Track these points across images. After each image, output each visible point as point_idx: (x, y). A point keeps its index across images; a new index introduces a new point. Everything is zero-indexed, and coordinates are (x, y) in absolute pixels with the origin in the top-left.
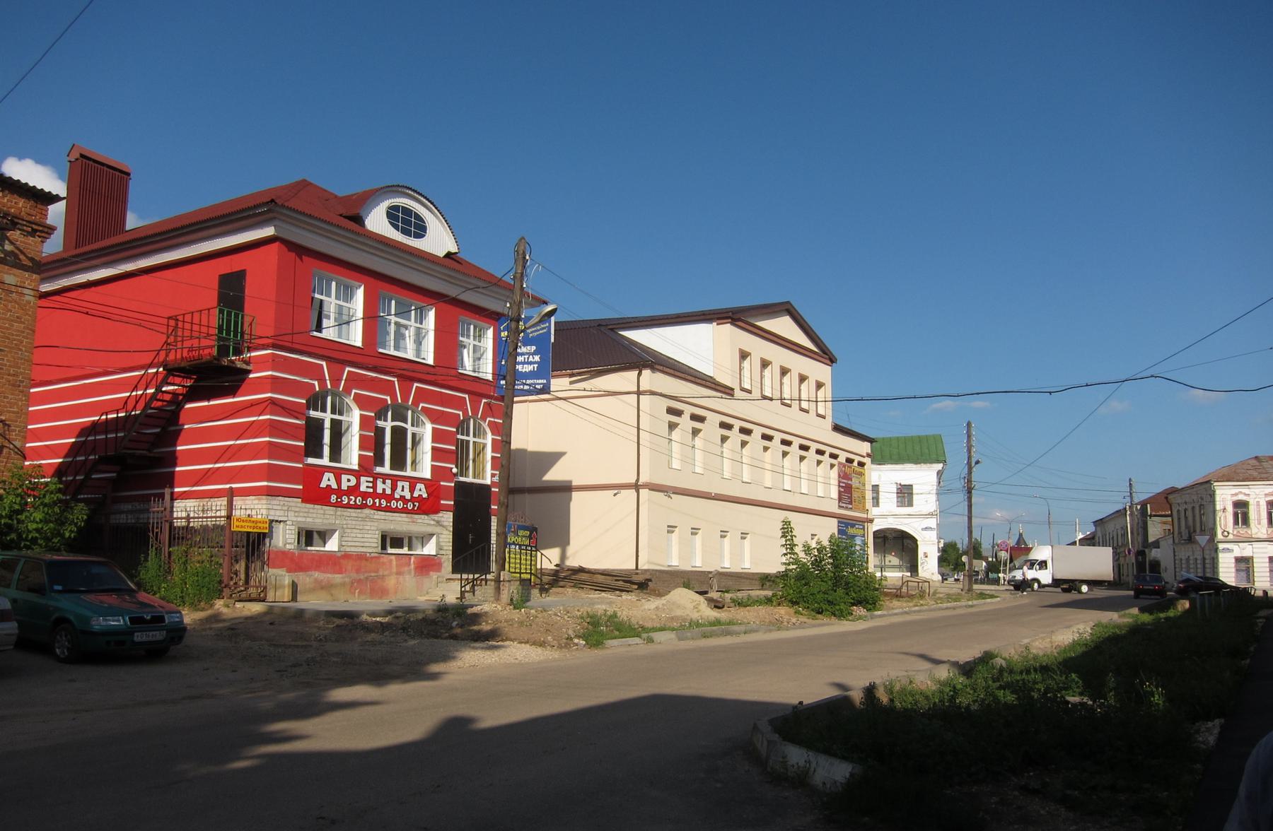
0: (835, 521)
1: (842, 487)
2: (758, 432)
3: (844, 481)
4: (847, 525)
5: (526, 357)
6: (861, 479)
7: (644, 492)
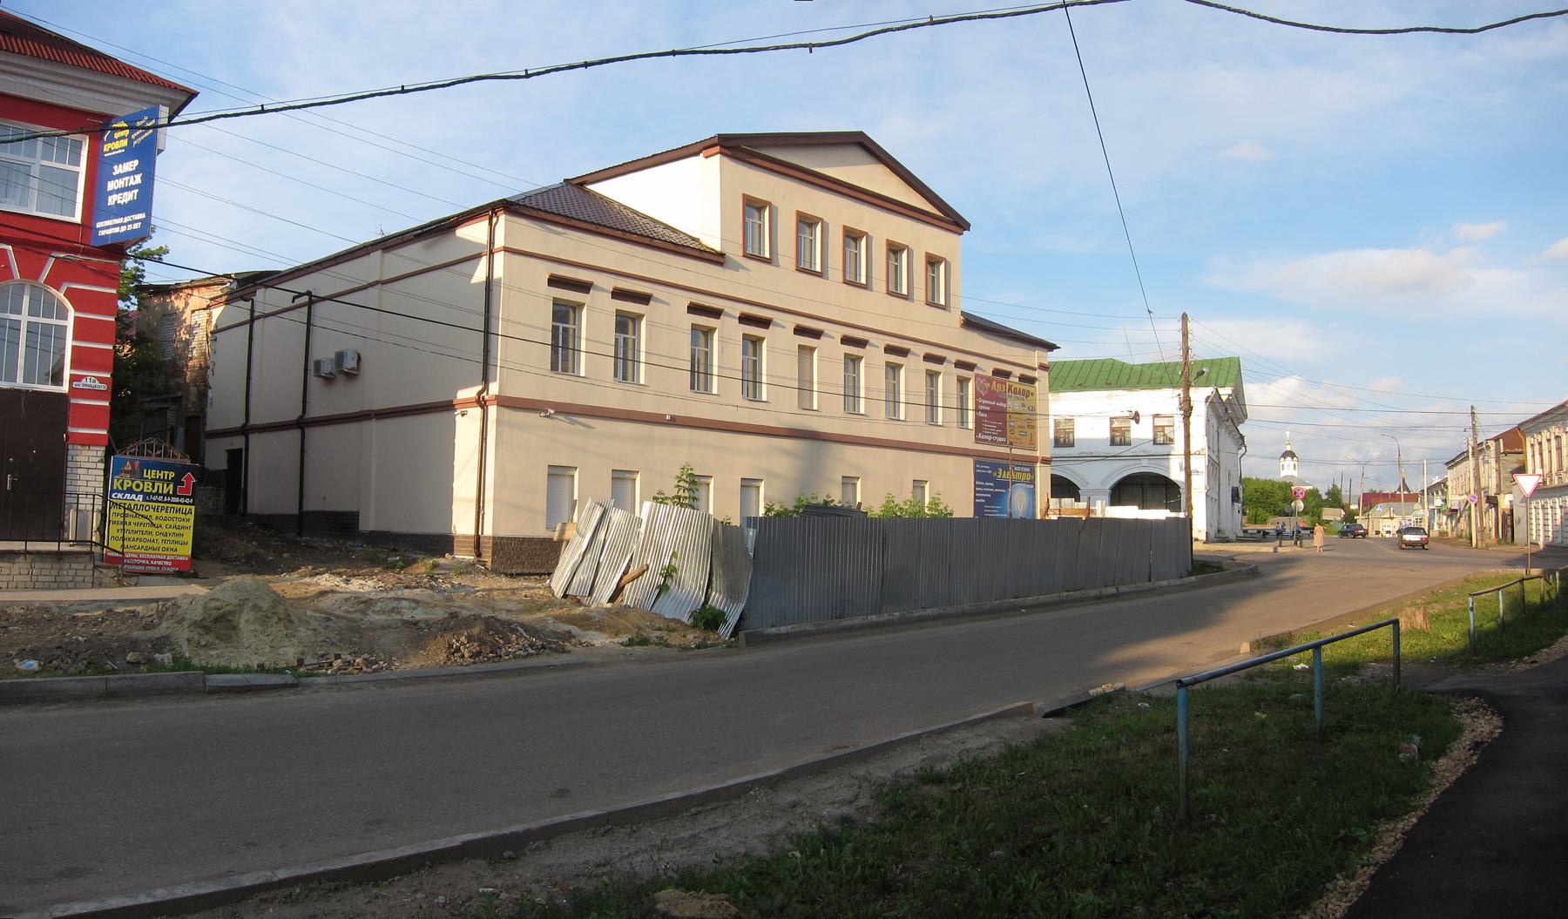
0: (970, 462)
1: (983, 411)
3: (988, 402)
4: (994, 467)
5: (127, 178)
6: (1028, 402)
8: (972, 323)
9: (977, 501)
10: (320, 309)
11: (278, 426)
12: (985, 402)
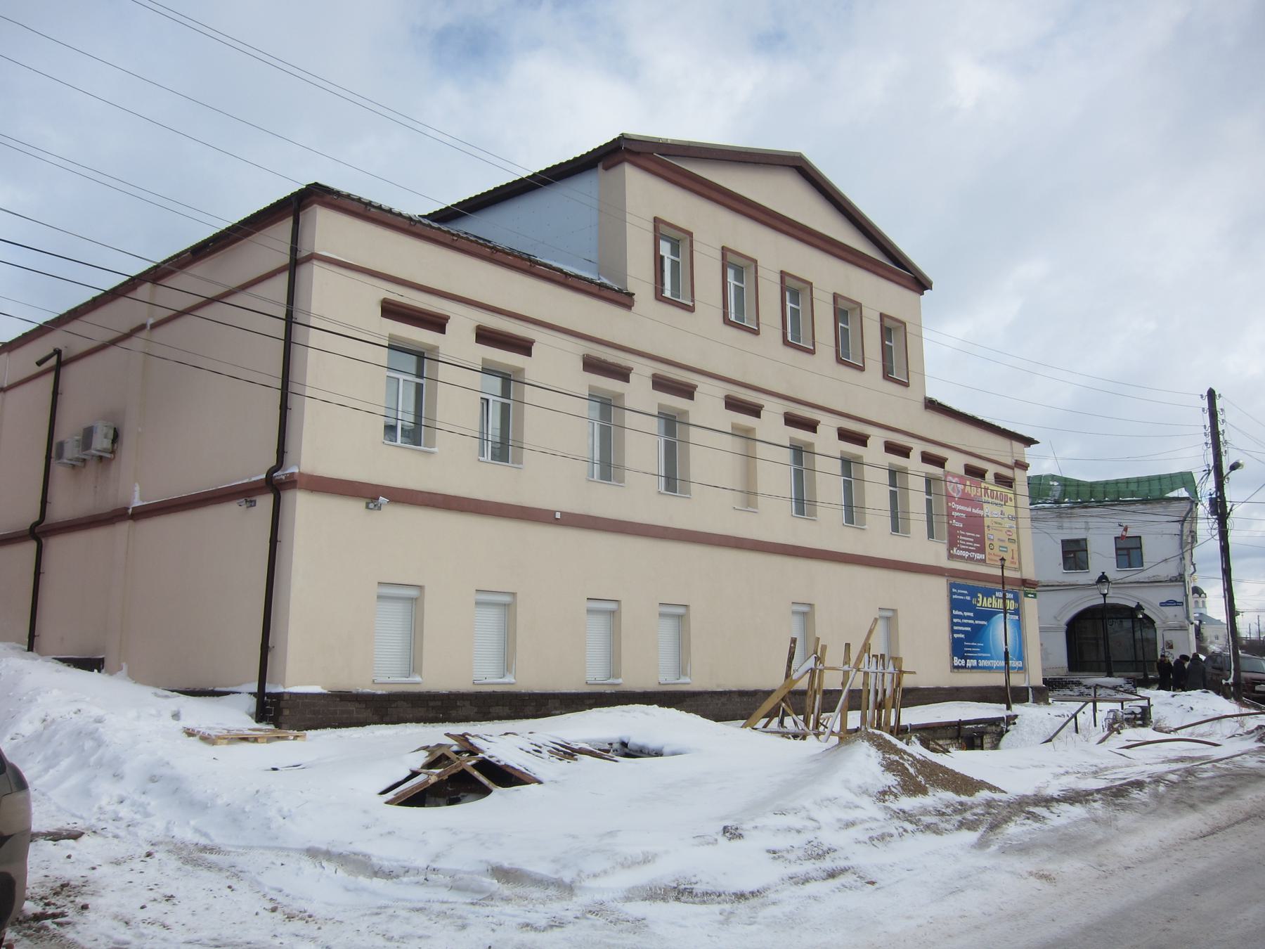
1: (959, 519)
2: (877, 439)
3: (962, 508)
4: (973, 592)
7: (302, 505)
8: (932, 405)
9: (956, 636)
10: (72, 374)
11: (20, 537)
12: (959, 507)
